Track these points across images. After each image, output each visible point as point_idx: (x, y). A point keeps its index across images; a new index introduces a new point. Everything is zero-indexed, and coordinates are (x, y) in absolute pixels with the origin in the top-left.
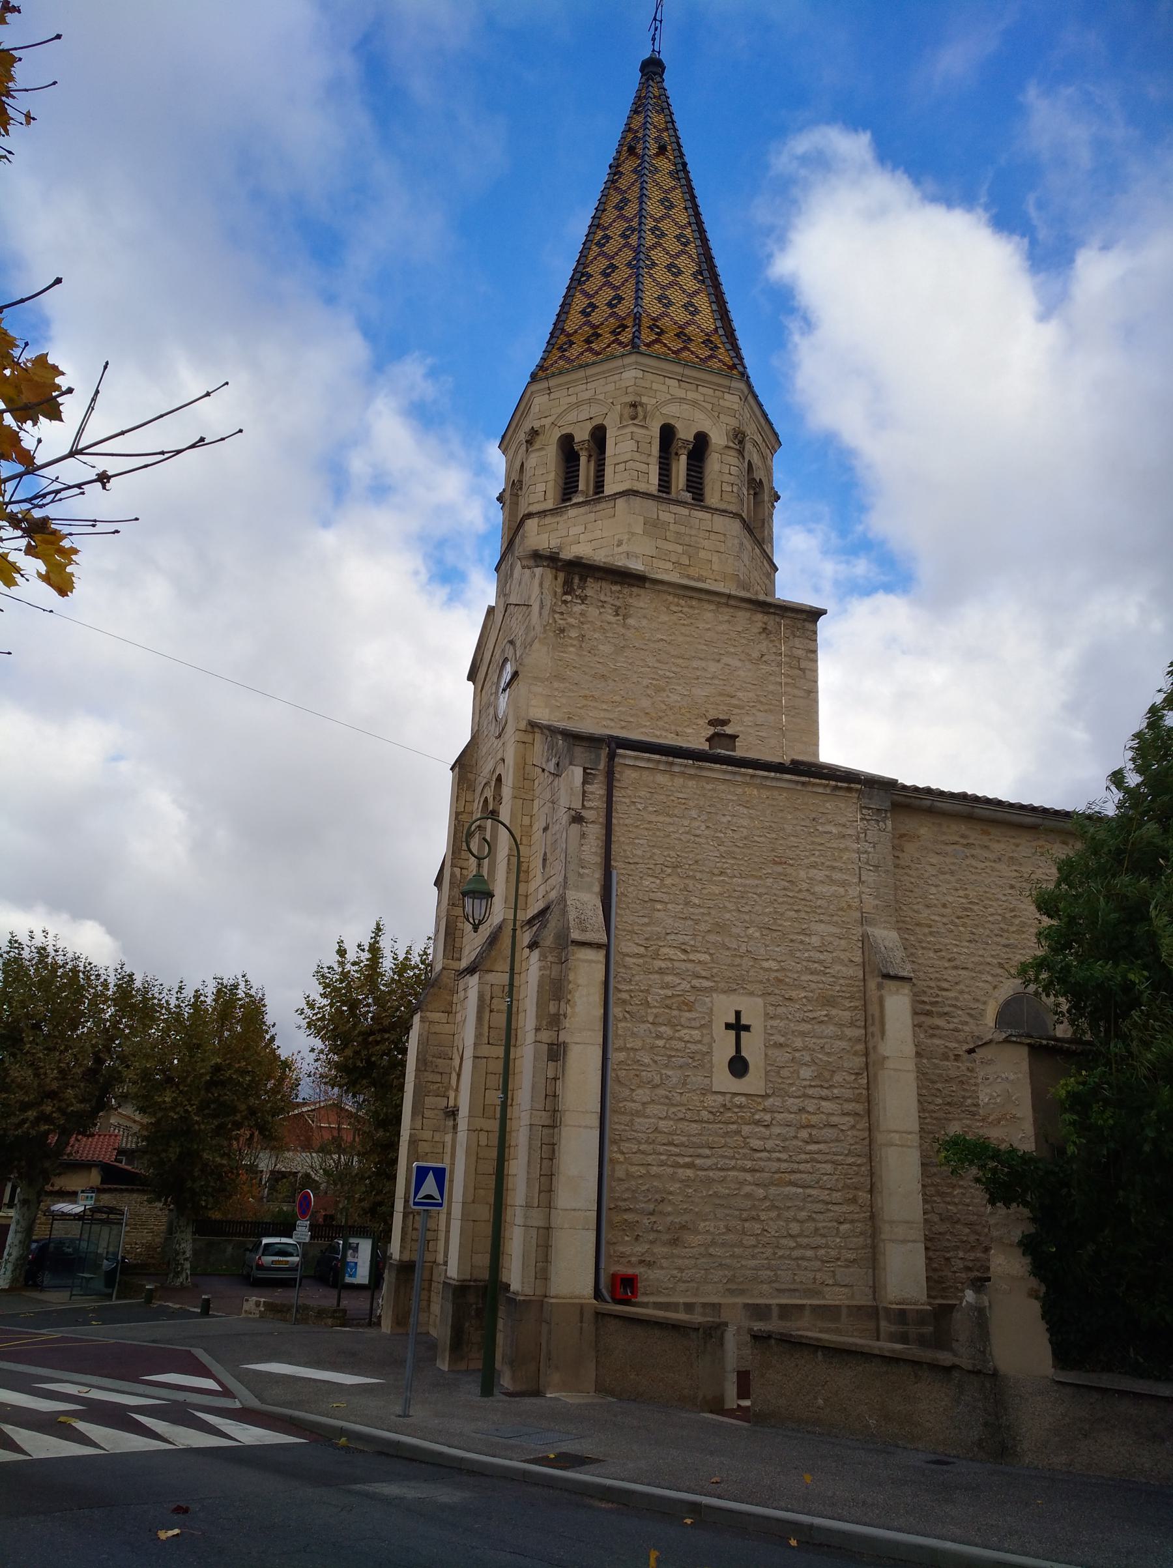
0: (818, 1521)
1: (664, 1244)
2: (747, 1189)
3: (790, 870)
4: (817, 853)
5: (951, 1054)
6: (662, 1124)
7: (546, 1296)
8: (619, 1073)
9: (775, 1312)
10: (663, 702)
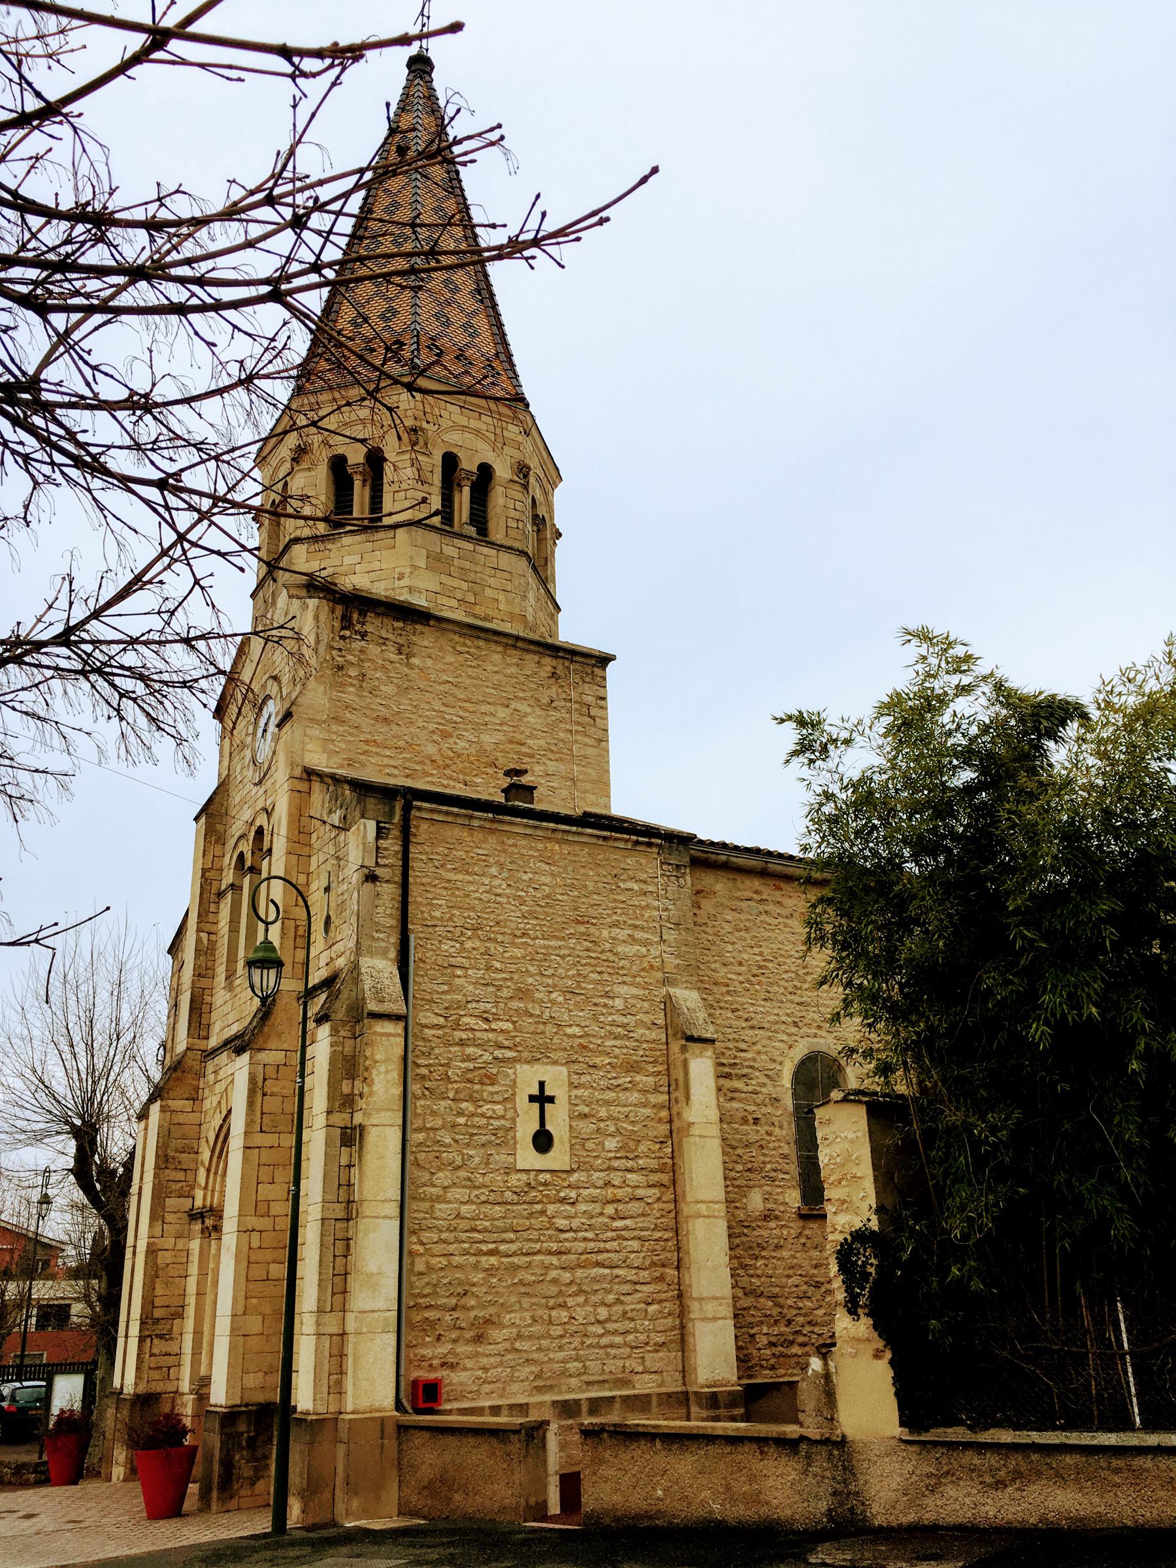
1: (468, 1342)
2: (553, 1274)
3: (592, 930)
4: (619, 911)
5: (750, 1118)
6: (464, 1209)
7: (341, 1413)
8: (418, 1156)
9: (585, 1408)
10: (450, 749)
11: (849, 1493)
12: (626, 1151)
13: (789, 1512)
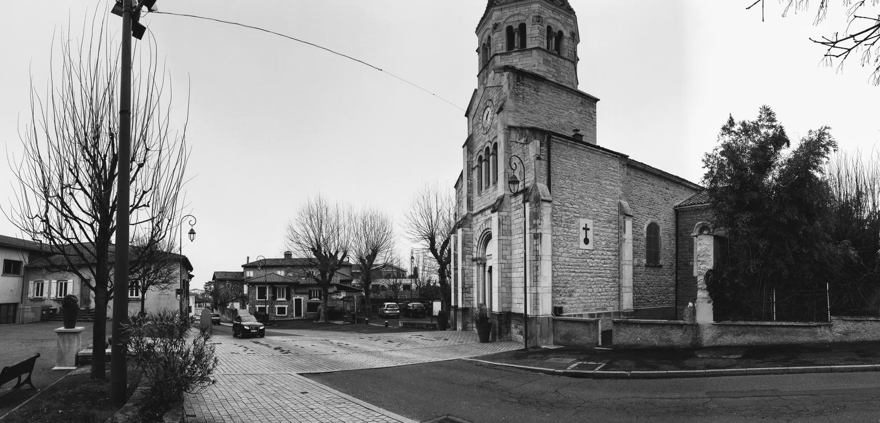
0: (854, 366)
2: (589, 279)
3: (600, 180)
11: (697, 338)
12: (607, 246)
13: (679, 344)
